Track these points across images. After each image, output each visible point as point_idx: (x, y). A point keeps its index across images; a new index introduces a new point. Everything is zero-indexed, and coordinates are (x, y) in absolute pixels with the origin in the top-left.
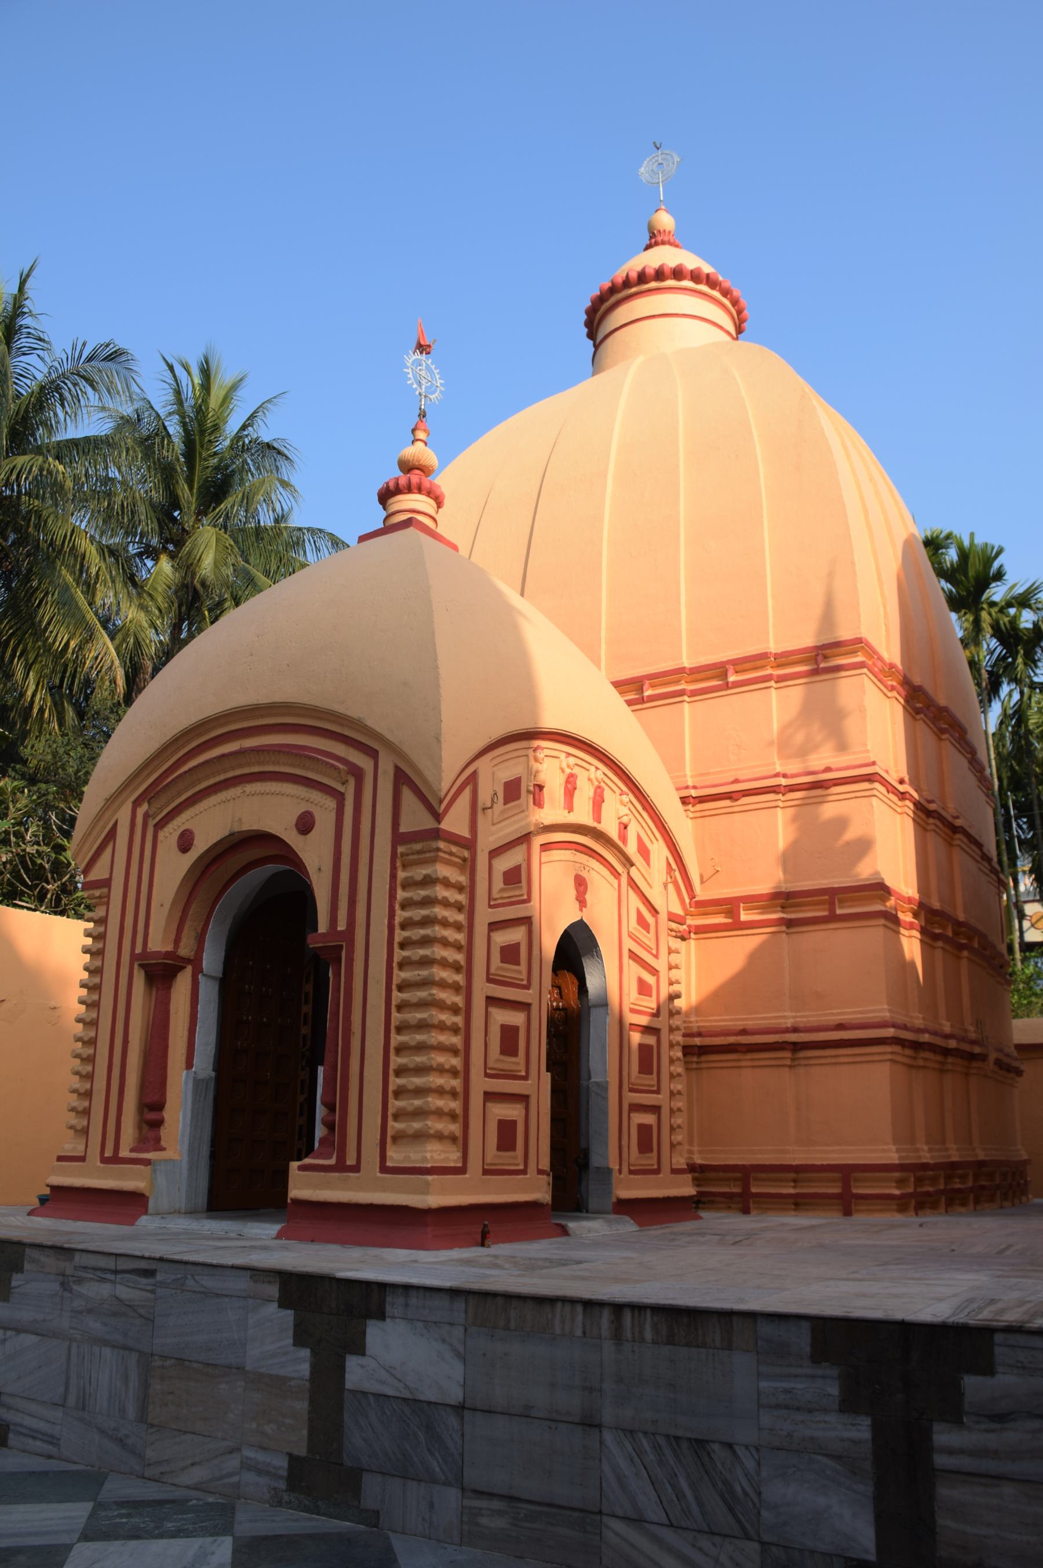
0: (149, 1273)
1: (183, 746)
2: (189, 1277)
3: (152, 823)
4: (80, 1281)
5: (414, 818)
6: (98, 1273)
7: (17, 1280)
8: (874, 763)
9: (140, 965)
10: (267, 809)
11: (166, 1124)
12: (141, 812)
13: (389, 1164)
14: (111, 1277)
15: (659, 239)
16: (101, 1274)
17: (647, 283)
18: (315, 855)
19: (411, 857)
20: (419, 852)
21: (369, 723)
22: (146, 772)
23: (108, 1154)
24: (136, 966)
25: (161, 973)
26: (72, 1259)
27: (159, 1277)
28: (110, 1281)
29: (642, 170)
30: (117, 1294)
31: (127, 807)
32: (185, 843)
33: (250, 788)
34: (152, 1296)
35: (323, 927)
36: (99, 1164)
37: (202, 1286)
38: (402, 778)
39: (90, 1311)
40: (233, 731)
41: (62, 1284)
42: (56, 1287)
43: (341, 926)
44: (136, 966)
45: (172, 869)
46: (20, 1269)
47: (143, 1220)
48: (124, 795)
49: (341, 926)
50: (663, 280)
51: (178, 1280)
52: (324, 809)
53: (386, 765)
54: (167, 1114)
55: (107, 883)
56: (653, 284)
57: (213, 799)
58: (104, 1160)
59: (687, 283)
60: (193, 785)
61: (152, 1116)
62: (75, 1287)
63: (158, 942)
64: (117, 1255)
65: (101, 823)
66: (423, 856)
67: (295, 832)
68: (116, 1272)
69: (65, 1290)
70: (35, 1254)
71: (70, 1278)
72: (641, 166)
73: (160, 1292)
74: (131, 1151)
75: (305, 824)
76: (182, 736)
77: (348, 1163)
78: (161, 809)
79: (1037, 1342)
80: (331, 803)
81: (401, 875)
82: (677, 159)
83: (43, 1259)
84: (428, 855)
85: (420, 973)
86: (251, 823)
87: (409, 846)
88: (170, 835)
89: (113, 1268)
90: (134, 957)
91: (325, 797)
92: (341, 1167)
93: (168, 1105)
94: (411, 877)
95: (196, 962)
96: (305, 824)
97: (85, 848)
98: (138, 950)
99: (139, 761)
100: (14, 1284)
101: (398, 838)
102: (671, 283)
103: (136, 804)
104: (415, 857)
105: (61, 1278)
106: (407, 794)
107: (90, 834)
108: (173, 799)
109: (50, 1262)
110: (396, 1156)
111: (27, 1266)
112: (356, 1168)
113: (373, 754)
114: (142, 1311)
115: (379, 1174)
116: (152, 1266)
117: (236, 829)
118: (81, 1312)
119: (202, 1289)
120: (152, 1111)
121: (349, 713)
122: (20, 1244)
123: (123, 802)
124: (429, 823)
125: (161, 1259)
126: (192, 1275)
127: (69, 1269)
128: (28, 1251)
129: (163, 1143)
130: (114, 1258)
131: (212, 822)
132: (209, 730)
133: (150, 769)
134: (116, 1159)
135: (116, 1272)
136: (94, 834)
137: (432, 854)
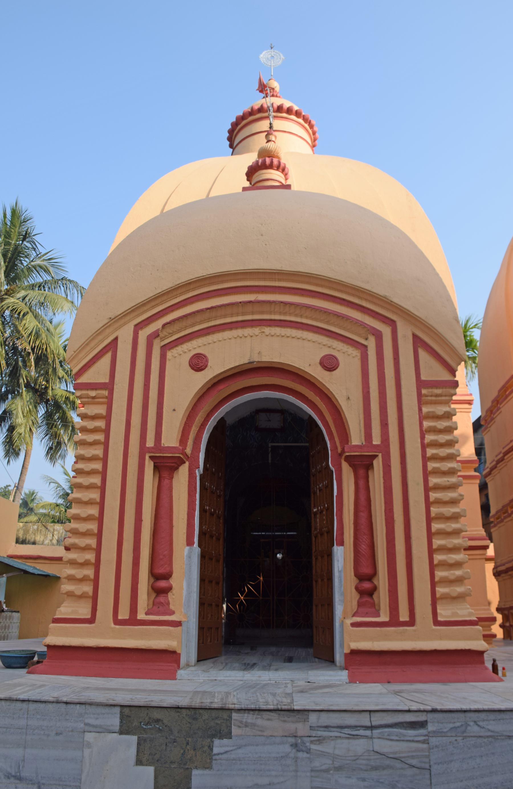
0: (423, 724)
1: (194, 289)
2: (472, 724)
3: (157, 345)
4: (320, 740)
5: (432, 370)
6: (346, 731)
7: (219, 746)
8: (471, 395)
9: (151, 458)
10: (298, 351)
11: (174, 591)
12: (144, 334)
13: (440, 619)
14: (368, 733)
15: (275, 94)
16: (351, 732)
17: (281, 113)
18: (344, 386)
19: (430, 398)
20: (437, 396)
21: (396, 300)
22: (153, 304)
23: (124, 614)
24: (147, 457)
25: (166, 466)
26: (306, 720)
27: (431, 727)
28: (366, 737)
29: (262, 56)
30: (376, 748)
31: (130, 328)
32: (198, 363)
33: (277, 330)
34: (425, 746)
35: (356, 438)
36: (113, 625)
37: (489, 730)
38: (418, 342)
39: (339, 769)
40: (247, 286)
41: (295, 745)
42: (287, 748)
43: (376, 441)
44: (147, 457)
45: (183, 387)
46: (229, 735)
47: (181, 673)
48: (128, 318)
49: (376, 441)
50: (290, 115)
51: (455, 728)
52: (348, 358)
53: (405, 332)
54: (174, 581)
55: (109, 386)
56: (284, 115)
57: (227, 334)
58: (117, 622)
59: (300, 120)
60: (209, 320)
61: (162, 584)
62: (313, 747)
63: (170, 439)
64: (370, 711)
65: (100, 337)
66: (440, 398)
67: (320, 368)
68: (372, 728)
69: (298, 751)
70: (249, 718)
71: (305, 739)
72: (261, 54)
73: (434, 741)
74: (147, 614)
75: (329, 364)
76: (278, 273)
77: (401, 619)
78: (171, 334)
79: (2, 696)
80: (356, 353)
81: (425, 410)
82: (282, 57)
83: (260, 722)
84: (443, 398)
85: (450, 480)
86: (334, 354)
87: (430, 390)
88: (180, 357)
89: (368, 724)
90: (143, 449)
91: (345, 345)
92: (394, 621)
93: (174, 575)
94: (433, 412)
95: (193, 460)
96: (329, 364)
97: (81, 355)
98: (150, 443)
99: (151, 294)
100: (216, 750)
101: (421, 384)
102: (293, 117)
103: (138, 327)
104: (433, 398)
105: (292, 740)
106: (423, 354)
107: (87, 344)
108: (186, 328)
109: (274, 725)
110: (445, 612)
111: (235, 731)
112: (411, 622)
113: (392, 323)
114: (414, 762)
115: (434, 627)
116: (422, 718)
117: (256, 359)
118: (327, 771)
119: (490, 734)
120: (161, 580)
121: (374, 290)
122: (226, 710)
123: (125, 324)
124: (446, 376)
125: (434, 711)
126: (475, 722)
127: (302, 729)
128: (235, 716)
129: (172, 607)
130: (367, 715)
131: (227, 352)
132: (222, 282)
133: (157, 302)
134: (133, 620)
135: (372, 728)
136: (92, 344)
137: (447, 398)
